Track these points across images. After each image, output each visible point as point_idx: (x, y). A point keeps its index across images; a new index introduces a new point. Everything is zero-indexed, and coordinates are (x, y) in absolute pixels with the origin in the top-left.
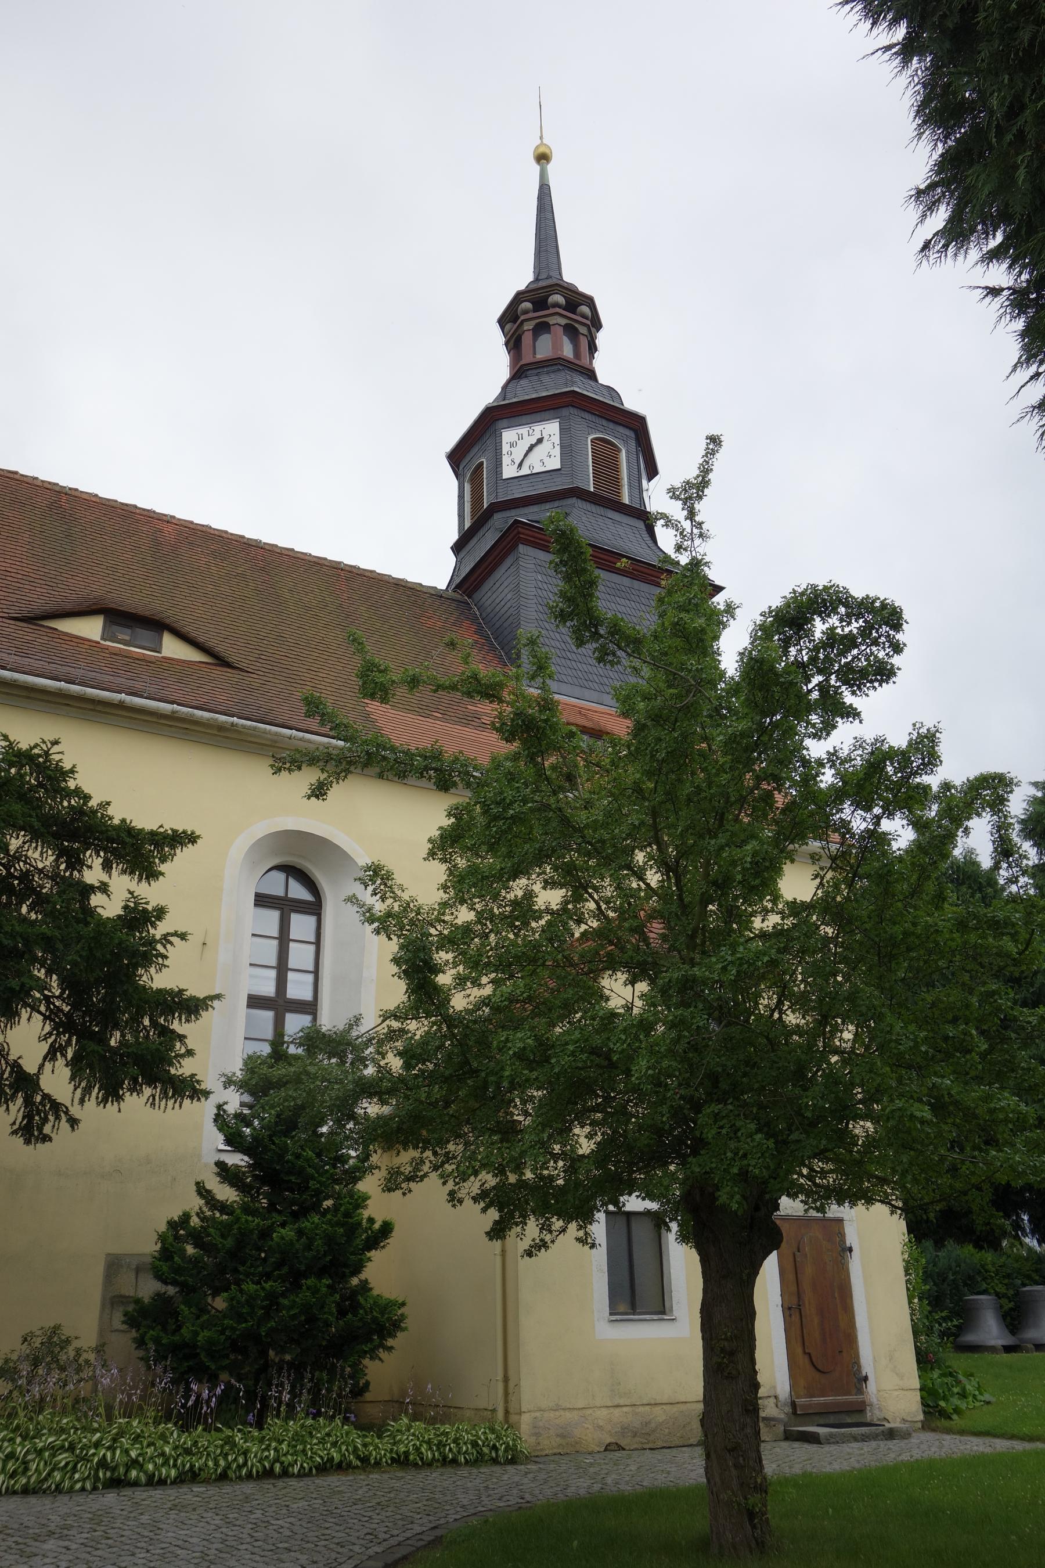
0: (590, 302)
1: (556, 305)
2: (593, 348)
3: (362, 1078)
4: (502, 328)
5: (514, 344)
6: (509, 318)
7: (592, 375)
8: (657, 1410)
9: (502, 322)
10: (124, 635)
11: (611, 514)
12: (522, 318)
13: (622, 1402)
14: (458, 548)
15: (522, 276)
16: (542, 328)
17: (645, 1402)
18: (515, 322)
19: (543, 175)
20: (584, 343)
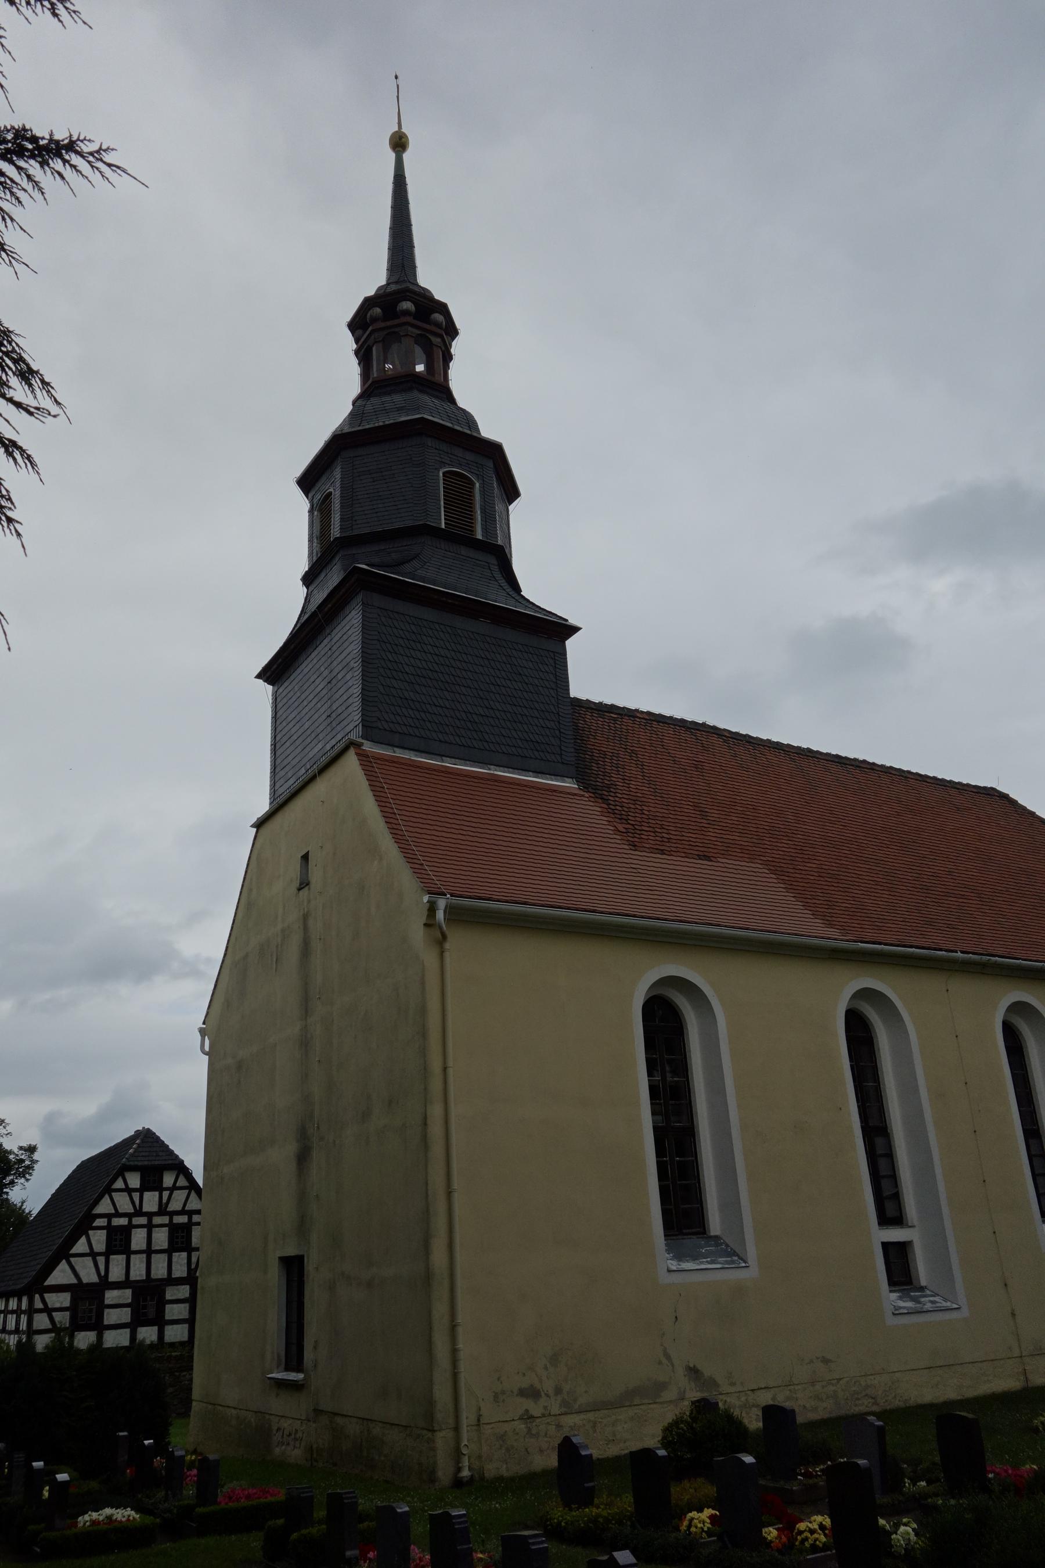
1: (406, 313)
2: (448, 357)
3: (393, 1509)
11: (464, 551)
14: (308, 579)
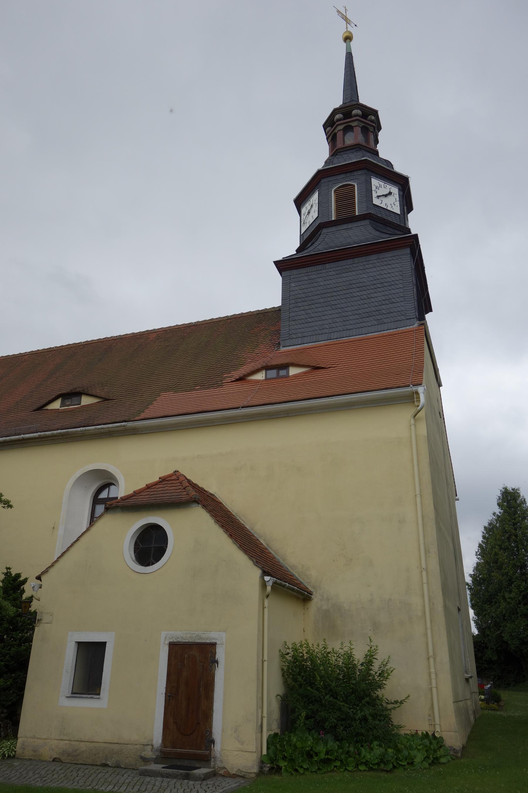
0: (375, 113)
4: (325, 130)
5: (332, 139)
6: (329, 124)
7: (376, 153)
8: (82, 744)
9: (325, 126)
12: (337, 123)
13: (64, 738)
15: (338, 101)
16: (348, 129)
17: (76, 739)
18: (332, 127)
19: (348, 48)
20: (372, 137)
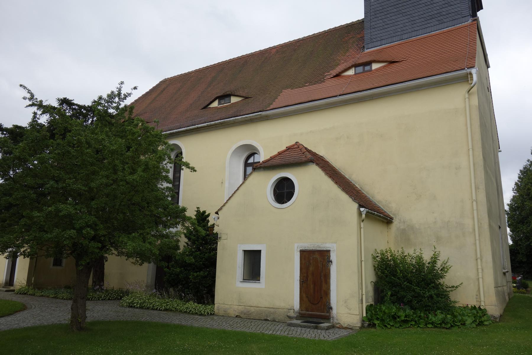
8: (252, 308)
10: (222, 102)
